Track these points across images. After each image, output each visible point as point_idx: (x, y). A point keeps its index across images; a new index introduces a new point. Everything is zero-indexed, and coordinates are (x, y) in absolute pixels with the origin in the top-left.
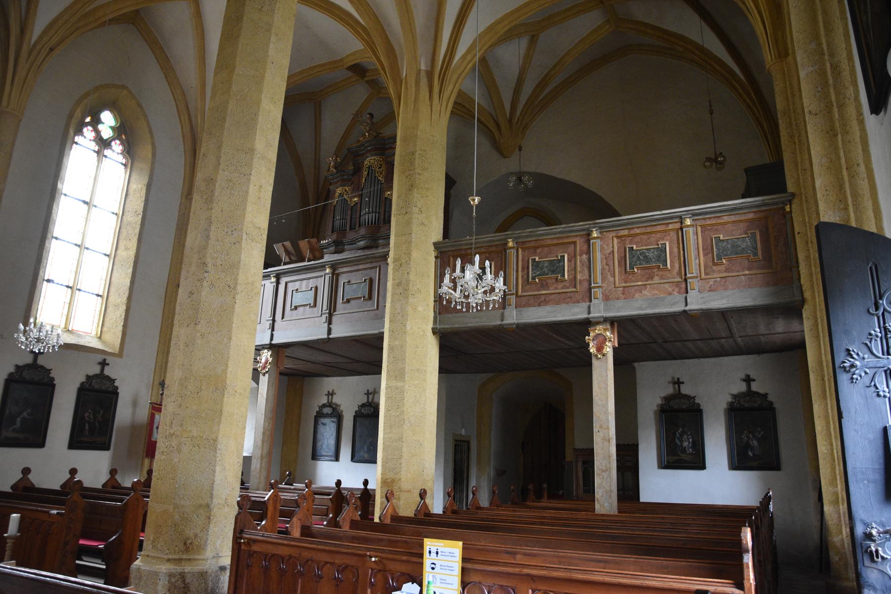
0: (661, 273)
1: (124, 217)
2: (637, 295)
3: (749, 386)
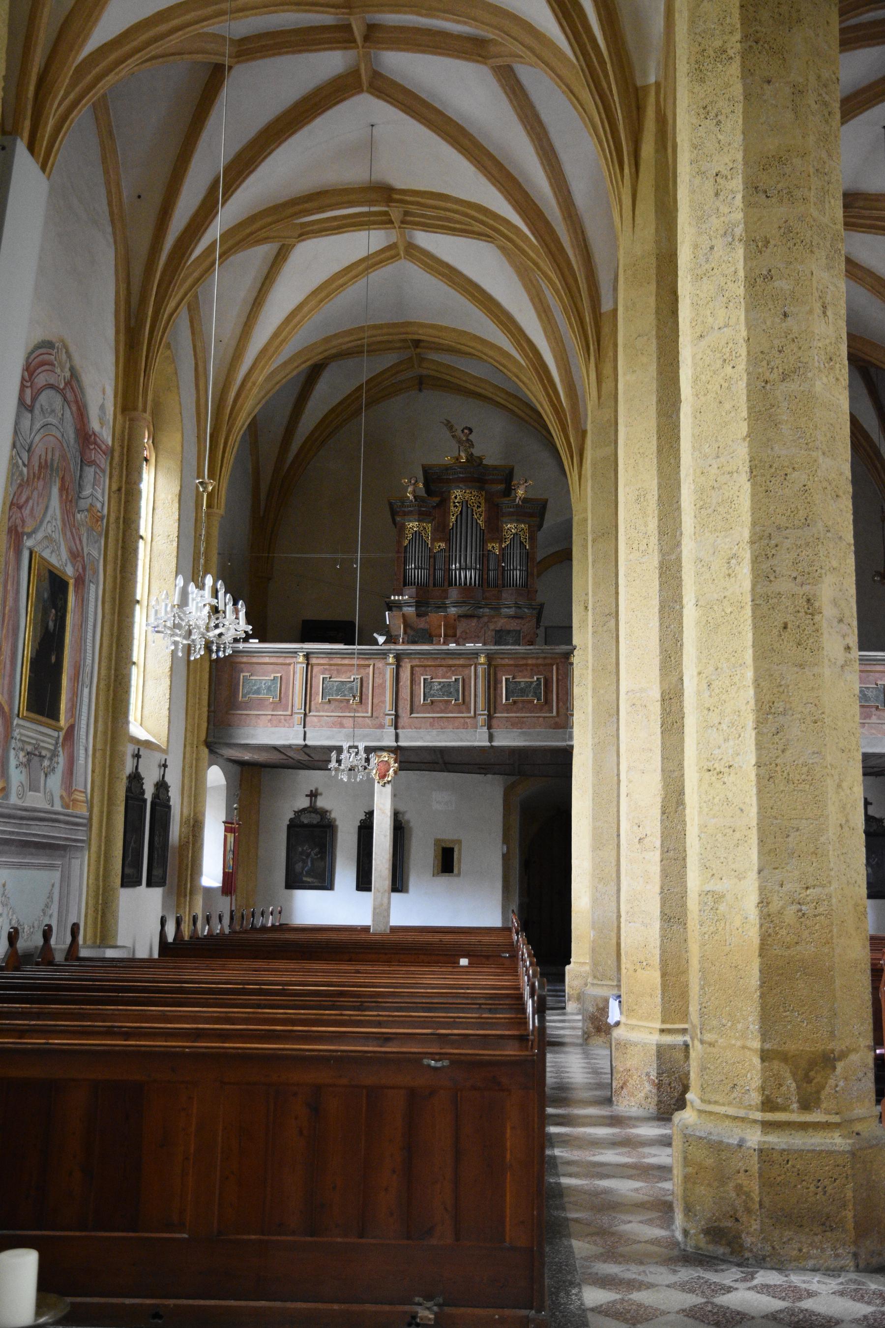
0: (878, 713)
1: (154, 543)
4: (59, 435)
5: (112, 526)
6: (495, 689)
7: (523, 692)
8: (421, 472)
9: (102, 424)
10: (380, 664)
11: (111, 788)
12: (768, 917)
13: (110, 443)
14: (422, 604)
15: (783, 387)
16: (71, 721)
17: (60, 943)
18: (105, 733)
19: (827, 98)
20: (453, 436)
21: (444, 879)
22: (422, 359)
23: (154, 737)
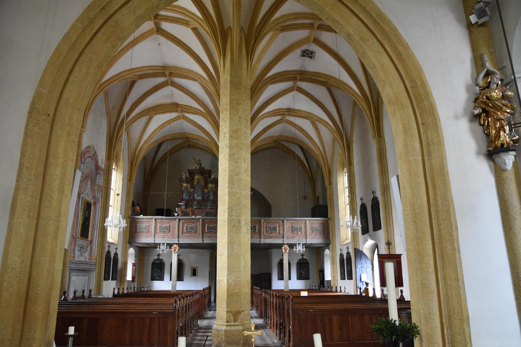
2: (295, 238)
3: (303, 257)
4: (90, 168)
5: (104, 189)
6: (204, 228)
7: (211, 229)
8: (187, 171)
9: (102, 164)
10: (174, 222)
11: (102, 255)
12: (228, 284)
13: (104, 168)
14: (187, 205)
15: (236, 177)
16: (91, 239)
17: (86, 294)
18: (100, 241)
19: (247, 118)
20: (196, 162)
21: (194, 278)
22: (189, 141)
23: (114, 241)
